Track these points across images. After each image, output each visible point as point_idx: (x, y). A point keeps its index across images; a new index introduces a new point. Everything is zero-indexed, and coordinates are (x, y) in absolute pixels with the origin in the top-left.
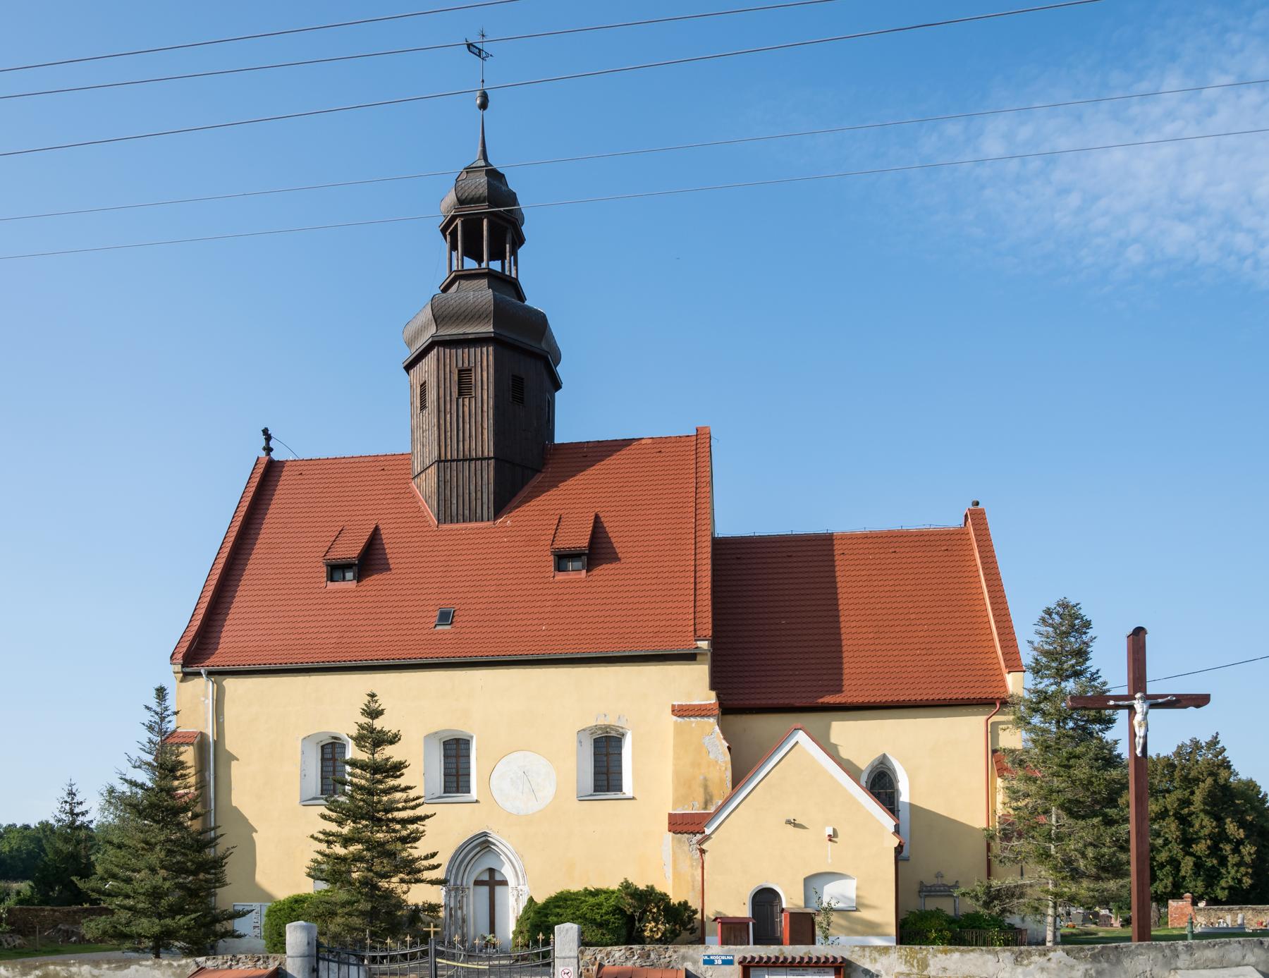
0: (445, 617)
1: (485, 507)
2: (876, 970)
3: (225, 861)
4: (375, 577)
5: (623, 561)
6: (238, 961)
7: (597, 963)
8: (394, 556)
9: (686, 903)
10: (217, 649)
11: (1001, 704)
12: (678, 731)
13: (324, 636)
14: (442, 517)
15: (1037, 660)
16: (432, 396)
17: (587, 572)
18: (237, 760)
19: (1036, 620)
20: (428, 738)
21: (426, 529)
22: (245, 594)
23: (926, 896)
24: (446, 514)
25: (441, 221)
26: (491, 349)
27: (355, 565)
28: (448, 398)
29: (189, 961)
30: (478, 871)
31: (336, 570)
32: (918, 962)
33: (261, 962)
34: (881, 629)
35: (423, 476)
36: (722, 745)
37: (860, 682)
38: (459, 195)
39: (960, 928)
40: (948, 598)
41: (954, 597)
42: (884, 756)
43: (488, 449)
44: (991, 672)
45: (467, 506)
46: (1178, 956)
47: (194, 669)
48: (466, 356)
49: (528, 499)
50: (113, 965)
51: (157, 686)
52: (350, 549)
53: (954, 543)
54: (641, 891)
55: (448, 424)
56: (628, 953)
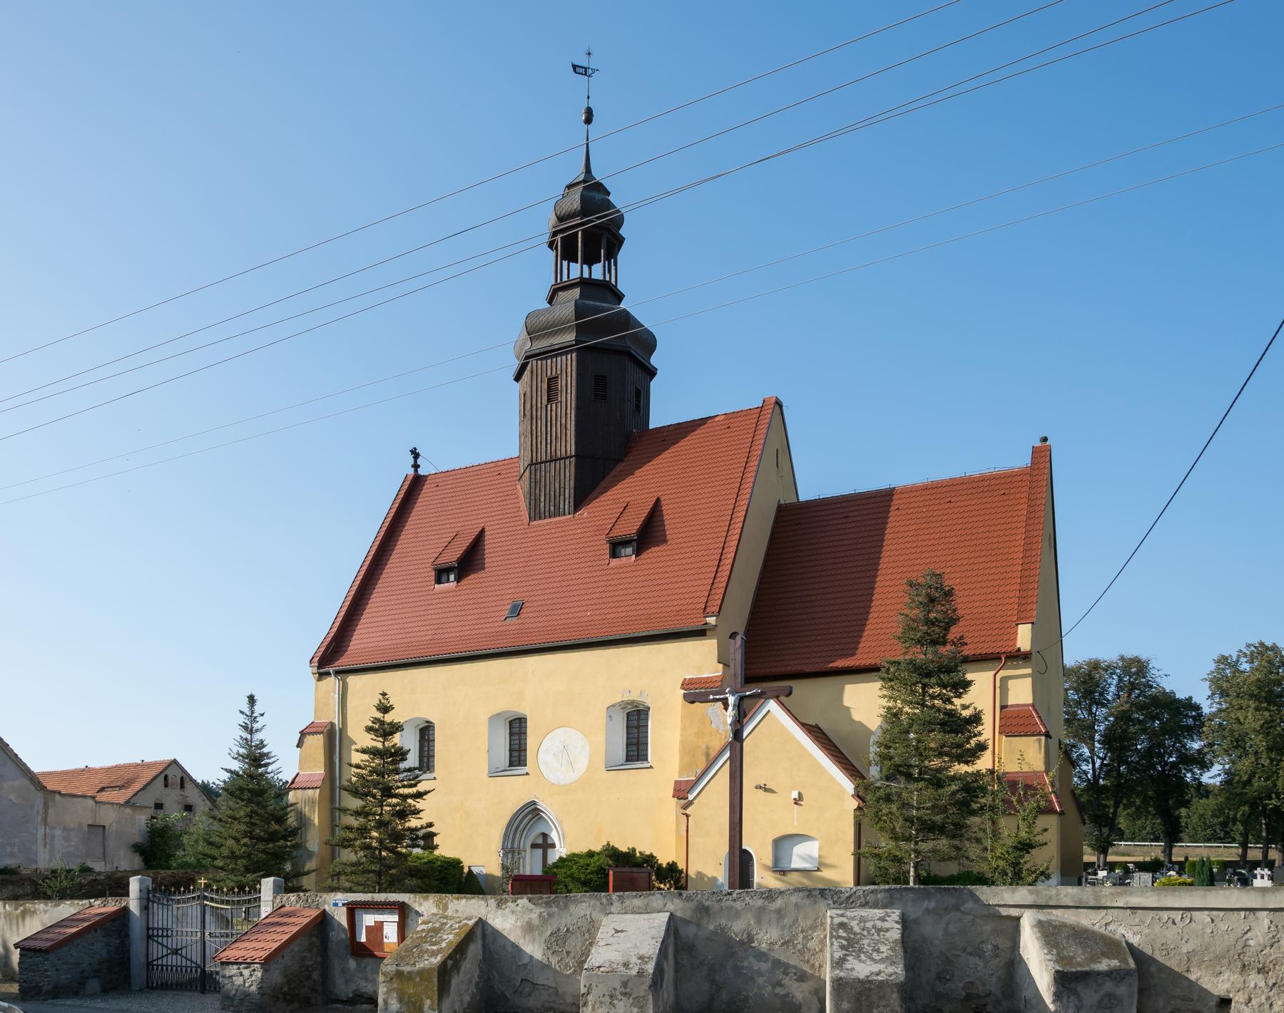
4: (653, 549)
11: (1007, 658)
14: (532, 515)
20: (494, 719)
28: (539, 405)
31: (441, 574)
43: (571, 448)
45: (552, 503)
47: (326, 669)
52: (452, 556)
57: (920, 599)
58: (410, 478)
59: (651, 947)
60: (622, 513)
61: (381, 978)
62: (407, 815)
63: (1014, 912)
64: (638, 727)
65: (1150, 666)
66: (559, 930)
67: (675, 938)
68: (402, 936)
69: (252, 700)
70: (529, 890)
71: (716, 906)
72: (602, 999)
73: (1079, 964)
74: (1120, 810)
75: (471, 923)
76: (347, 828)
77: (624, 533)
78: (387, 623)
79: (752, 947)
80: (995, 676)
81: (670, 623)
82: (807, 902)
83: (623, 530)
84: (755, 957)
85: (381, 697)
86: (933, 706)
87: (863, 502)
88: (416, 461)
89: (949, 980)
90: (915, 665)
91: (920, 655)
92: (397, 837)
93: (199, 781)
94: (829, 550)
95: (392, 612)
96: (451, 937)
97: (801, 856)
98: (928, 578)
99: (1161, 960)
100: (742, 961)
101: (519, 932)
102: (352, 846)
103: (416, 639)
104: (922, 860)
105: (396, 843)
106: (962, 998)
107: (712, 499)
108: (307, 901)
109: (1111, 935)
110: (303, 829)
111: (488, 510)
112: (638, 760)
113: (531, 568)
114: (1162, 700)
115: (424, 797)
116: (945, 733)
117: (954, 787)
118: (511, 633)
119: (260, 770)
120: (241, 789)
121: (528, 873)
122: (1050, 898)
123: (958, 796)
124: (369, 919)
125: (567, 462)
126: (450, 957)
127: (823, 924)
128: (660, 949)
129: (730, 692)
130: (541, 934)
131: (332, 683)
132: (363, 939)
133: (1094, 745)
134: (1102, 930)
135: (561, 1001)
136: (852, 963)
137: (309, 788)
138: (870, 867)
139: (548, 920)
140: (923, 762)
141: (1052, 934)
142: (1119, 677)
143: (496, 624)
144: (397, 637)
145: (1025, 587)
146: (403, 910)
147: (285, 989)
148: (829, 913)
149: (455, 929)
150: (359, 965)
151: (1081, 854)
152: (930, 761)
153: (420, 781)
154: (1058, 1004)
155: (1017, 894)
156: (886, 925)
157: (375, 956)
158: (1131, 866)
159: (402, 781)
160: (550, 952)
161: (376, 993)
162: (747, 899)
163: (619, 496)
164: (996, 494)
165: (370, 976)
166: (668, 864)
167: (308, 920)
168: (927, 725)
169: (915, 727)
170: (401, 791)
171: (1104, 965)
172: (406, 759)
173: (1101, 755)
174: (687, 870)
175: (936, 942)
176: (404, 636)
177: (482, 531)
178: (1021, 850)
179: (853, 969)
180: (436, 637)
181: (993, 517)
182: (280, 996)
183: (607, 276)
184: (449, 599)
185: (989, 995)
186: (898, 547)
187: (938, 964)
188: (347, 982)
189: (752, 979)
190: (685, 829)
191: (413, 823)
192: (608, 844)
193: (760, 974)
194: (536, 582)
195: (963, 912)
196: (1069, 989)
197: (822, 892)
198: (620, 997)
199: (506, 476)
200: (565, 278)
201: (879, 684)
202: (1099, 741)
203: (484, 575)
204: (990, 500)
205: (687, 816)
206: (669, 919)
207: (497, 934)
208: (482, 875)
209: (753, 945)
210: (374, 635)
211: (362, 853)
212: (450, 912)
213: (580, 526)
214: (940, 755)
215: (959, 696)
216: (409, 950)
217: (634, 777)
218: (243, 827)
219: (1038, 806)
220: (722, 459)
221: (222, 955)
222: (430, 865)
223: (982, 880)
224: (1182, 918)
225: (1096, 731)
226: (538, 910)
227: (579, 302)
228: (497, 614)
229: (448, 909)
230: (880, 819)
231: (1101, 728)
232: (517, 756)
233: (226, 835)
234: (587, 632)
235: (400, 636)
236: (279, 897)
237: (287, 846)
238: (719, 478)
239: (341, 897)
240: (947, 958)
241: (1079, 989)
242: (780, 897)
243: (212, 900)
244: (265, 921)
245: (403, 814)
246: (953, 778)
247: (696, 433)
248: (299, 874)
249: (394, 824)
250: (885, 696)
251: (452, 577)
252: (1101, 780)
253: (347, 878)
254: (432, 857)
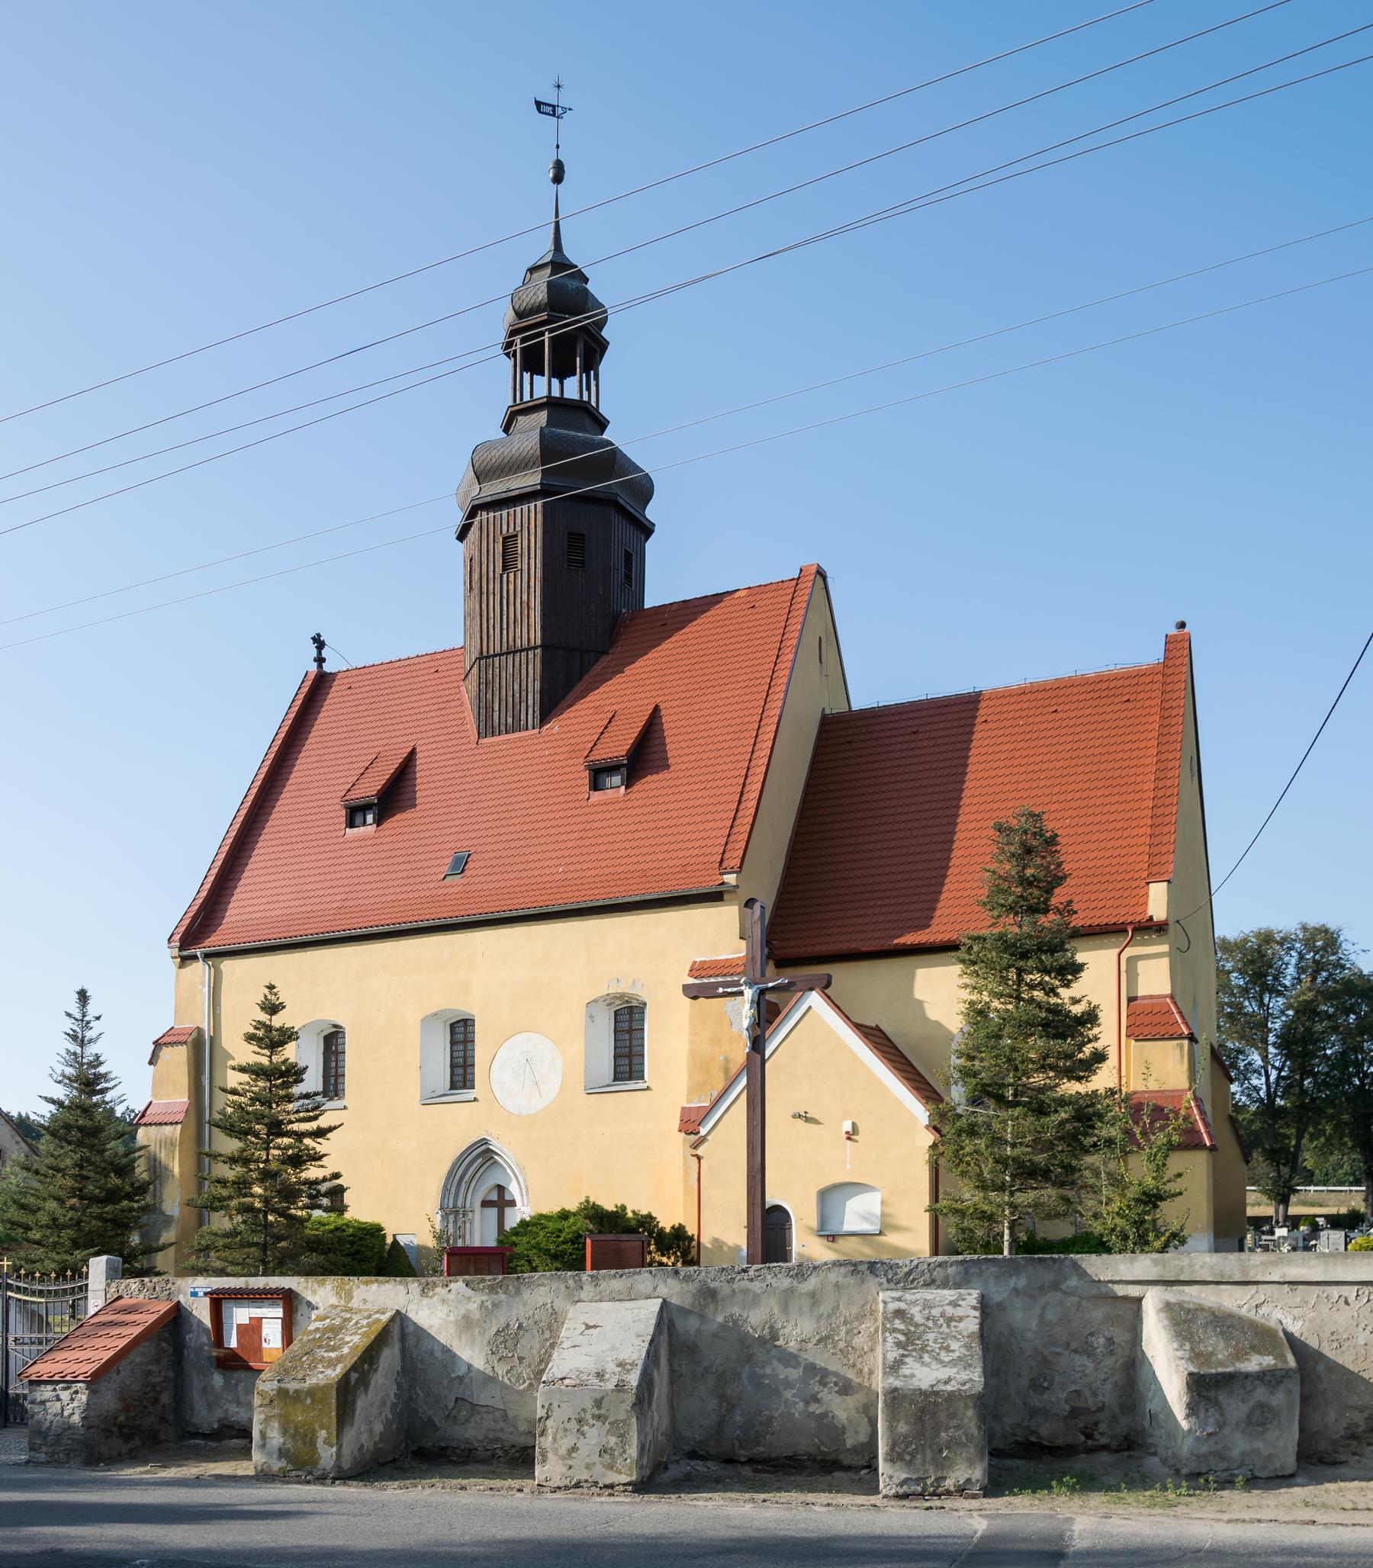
4: (649, 778)
11: (1135, 930)
14: (482, 730)
20: (428, 1020)
27: (375, 804)
30: (484, 1190)
31: (354, 814)
38: (517, 307)
43: (536, 636)
45: (510, 713)
46: (582, 1288)
47: (192, 952)
51: (78, 988)
52: (370, 788)
57: (1012, 849)
58: (311, 677)
59: (635, 1350)
60: (606, 728)
61: (257, 1401)
62: (304, 1162)
63: (1134, 1291)
64: (630, 1031)
65: (1342, 938)
66: (508, 1325)
67: (670, 1336)
68: (288, 1338)
69: (83, 996)
70: (472, 1269)
71: (725, 1289)
72: (567, 1425)
73: (1221, 1363)
74: (1304, 1141)
75: (385, 1318)
76: (218, 1181)
77: (616, 754)
78: (278, 884)
79: (776, 1346)
80: (1119, 955)
81: (701, 879)
82: (851, 1280)
83: (608, 750)
84: (780, 1360)
85: (267, 991)
86: (1032, 1000)
87: (938, 711)
88: (320, 653)
89: (1047, 1388)
90: (1006, 941)
91: (1013, 927)
92: (290, 1194)
93: (14, 1114)
94: (906, 777)
95: (285, 869)
96: (356, 1338)
97: (858, 1213)
98: (1023, 819)
99: (1331, 1355)
100: (763, 1367)
101: (452, 1330)
102: (227, 1208)
103: (319, 907)
104: (1020, 1218)
105: (288, 1202)
106: (1065, 1414)
107: (732, 708)
108: (155, 1288)
109: (1263, 1321)
110: (157, 1182)
111: (422, 722)
112: (630, 1079)
113: (480, 805)
114: (1357, 986)
115: (329, 1135)
116: (1048, 1037)
117: (1064, 1115)
118: (452, 897)
119: (94, 1099)
120: (68, 1127)
121: (477, 1244)
122: (1182, 1270)
123: (1068, 1126)
124: (241, 1315)
125: (531, 655)
126: (354, 1368)
127: (872, 1312)
128: (648, 1352)
129: (745, 983)
130: (482, 1333)
131: (199, 970)
132: (234, 1344)
133: (1266, 1050)
134: (1252, 1315)
135: (512, 1429)
136: (911, 1366)
137: (166, 1124)
138: (950, 1229)
139: (492, 1311)
140: (1020, 1079)
141: (1185, 1322)
142: (1300, 953)
143: (432, 885)
144: (292, 903)
145: (1157, 831)
146: (289, 1300)
147: (122, 1418)
148: (881, 1296)
149: (363, 1327)
150: (227, 1381)
151: (1244, 1206)
152: (1028, 1078)
153: (325, 1111)
154: (1193, 1419)
155: (1137, 1265)
156: (959, 1312)
157: (251, 1369)
158: (1321, 1221)
159: (298, 1112)
160: (495, 1358)
161: (251, 1421)
162: (769, 1277)
163: (602, 703)
164: (1117, 700)
165: (242, 1398)
166: (673, 1227)
167: (155, 1317)
168: (1025, 1027)
169: (1007, 1030)
170: (295, 1127)
171: (1254, 1364)
172: (302, 1081)
173: (1277, 1064)
174: (699, 1236)
175: (1029, 1335)
176: (302, 902)
177: (413, 753)
178: (1146, 1203)
179: (912, 1376)
180: (347, 904)
181: (1113, 732)
182: (115, 1429)
183: (585, 393)
184: (365, 850)
185: (1101, 1409)
186: (987, 774)
187: (1031, 1367)
188: (210, 1406)
189: (777, 1392)
190: (696, 1176)
191: (312, 1172)
192: (587, 1201)
193: (788, 1384)
194: (488, 825)
195: (1064, 1292)
196: (1208, 1399)
197: (872, 1266)
198: (591, 1422)
199: (447, 674)
200: (527, 397)
201: (958, 968)
202: (1274, 1044)
203: (415, 815)
204: (1110, 708)
205: (699, 1158)
206: (662, 1308)
207: (421, 1333)
208: (413, 1248)
209: (777, 1343)
210: (260, 901)
211: (240, 1218)
212: (355, 1303)
213: (549, 745)
214: (1043, 1068)
215: (1067, 985)
216: (296, 1359)
217: (626, 1101)
218: (69, 1182)
219: (1170, 1142)
220: (743, 651)
221: (31, 1371)
222: (338, 1234)
223: (1101, 1247)
224: (1358, 1295)
225: (1270, 1030)
226: (478, 1298)
227: (546, 431)
228: (433, 870)
229: (352, 1298)
230: (961, 1160)
231: (1277, 1026)
232: (462, 1075)
233: (46, 1195)
234: (558, 896)
235: (297, 903)
236: (114, 1285)
237: (132, 1210)
238: (740, 678)
239: (206, 1283)
240: (1045, 1357)
241: (1221, 1398)
242: (814, 1274)
243: (18, 1290)
244: (93, 1321)
245: (298, 1161)
246: (1062, 1102)
247: (708, 614)
248: (149, 1250)
249: (284, 1175)
250: (966, 986)
251: (370, 818)
252: (1278, 1099)
253: (218, 1254)
254: (340, 1222)
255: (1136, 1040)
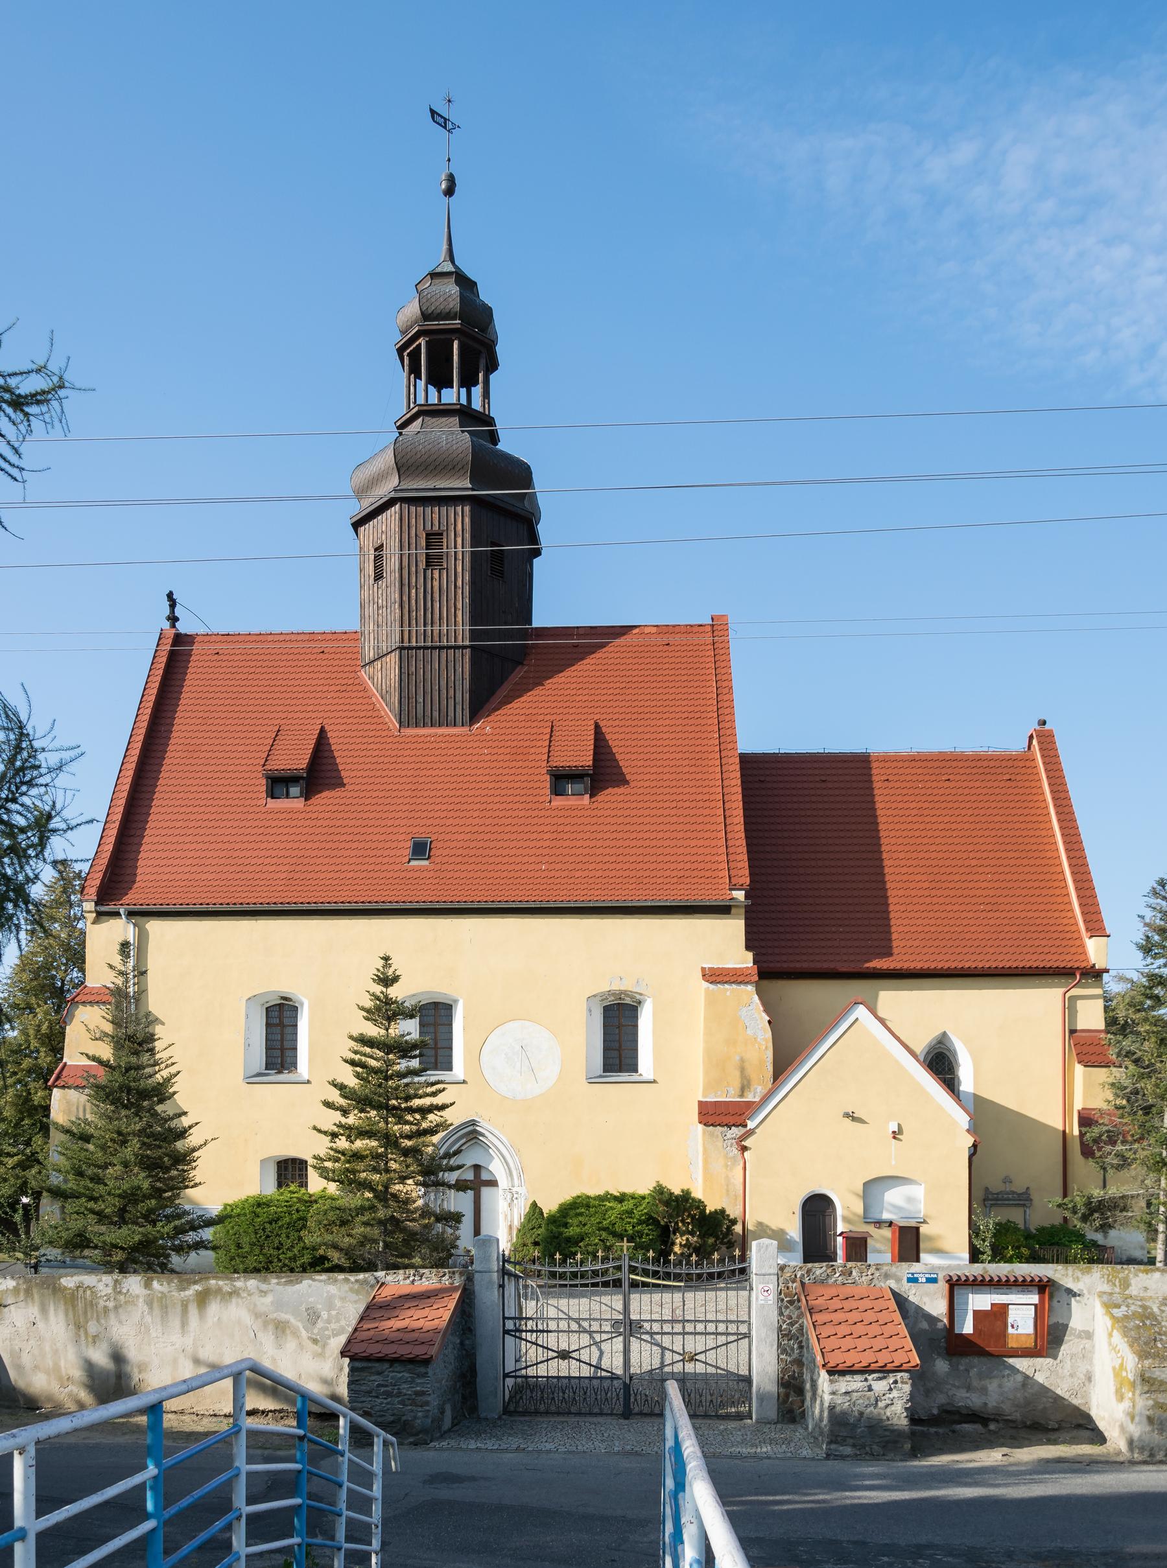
0: (420, 849)
1: (459, 708)
2: (1079, 1290)
3: (196, 1154)
4: (325, 794)
5: (632, 784)
6: (421, 1276)
7: (798, 1280)
8: (348, 767)
9: (723, 1211)
10: (134, 882)
11: (1082, 974)
12: (710, 1001)
13: (272, 869)
14: (405, 718)
15: (1148, 937)
16: (392, 564)
17: (591, 797)
18: (163, 1024)
19: (1148, 889)
21: (384, 734)
22: (163, 810)
23: (992, 1205)
24: (408, 717)
25: (397, 338)
26: (467, 509)
27: (302, 778)
28: (413, 569)
29: (367, 1275)
31: (278, 784)
32: (1120, 1281)
33: (447, 1277)
34: (937, 878)
35: (378, 664)
36: (762, 1018)
37: (916, 943)
39: (1040, 1245)
40: (1014, 840)
41: (1020, 840)
42: (944, 1034)
44: (1069, 936)
48: (436, 516)
49: (508, 700)
50: (283, 1280)
52: (296, 759)
53: (1017, 771)
54: (677, 1197)
55: (413, 602)
56: (829, 1271)
88: (172, 611)
124: (981, 1301)
165: (975, 1383)
255: (1085, 1066)
